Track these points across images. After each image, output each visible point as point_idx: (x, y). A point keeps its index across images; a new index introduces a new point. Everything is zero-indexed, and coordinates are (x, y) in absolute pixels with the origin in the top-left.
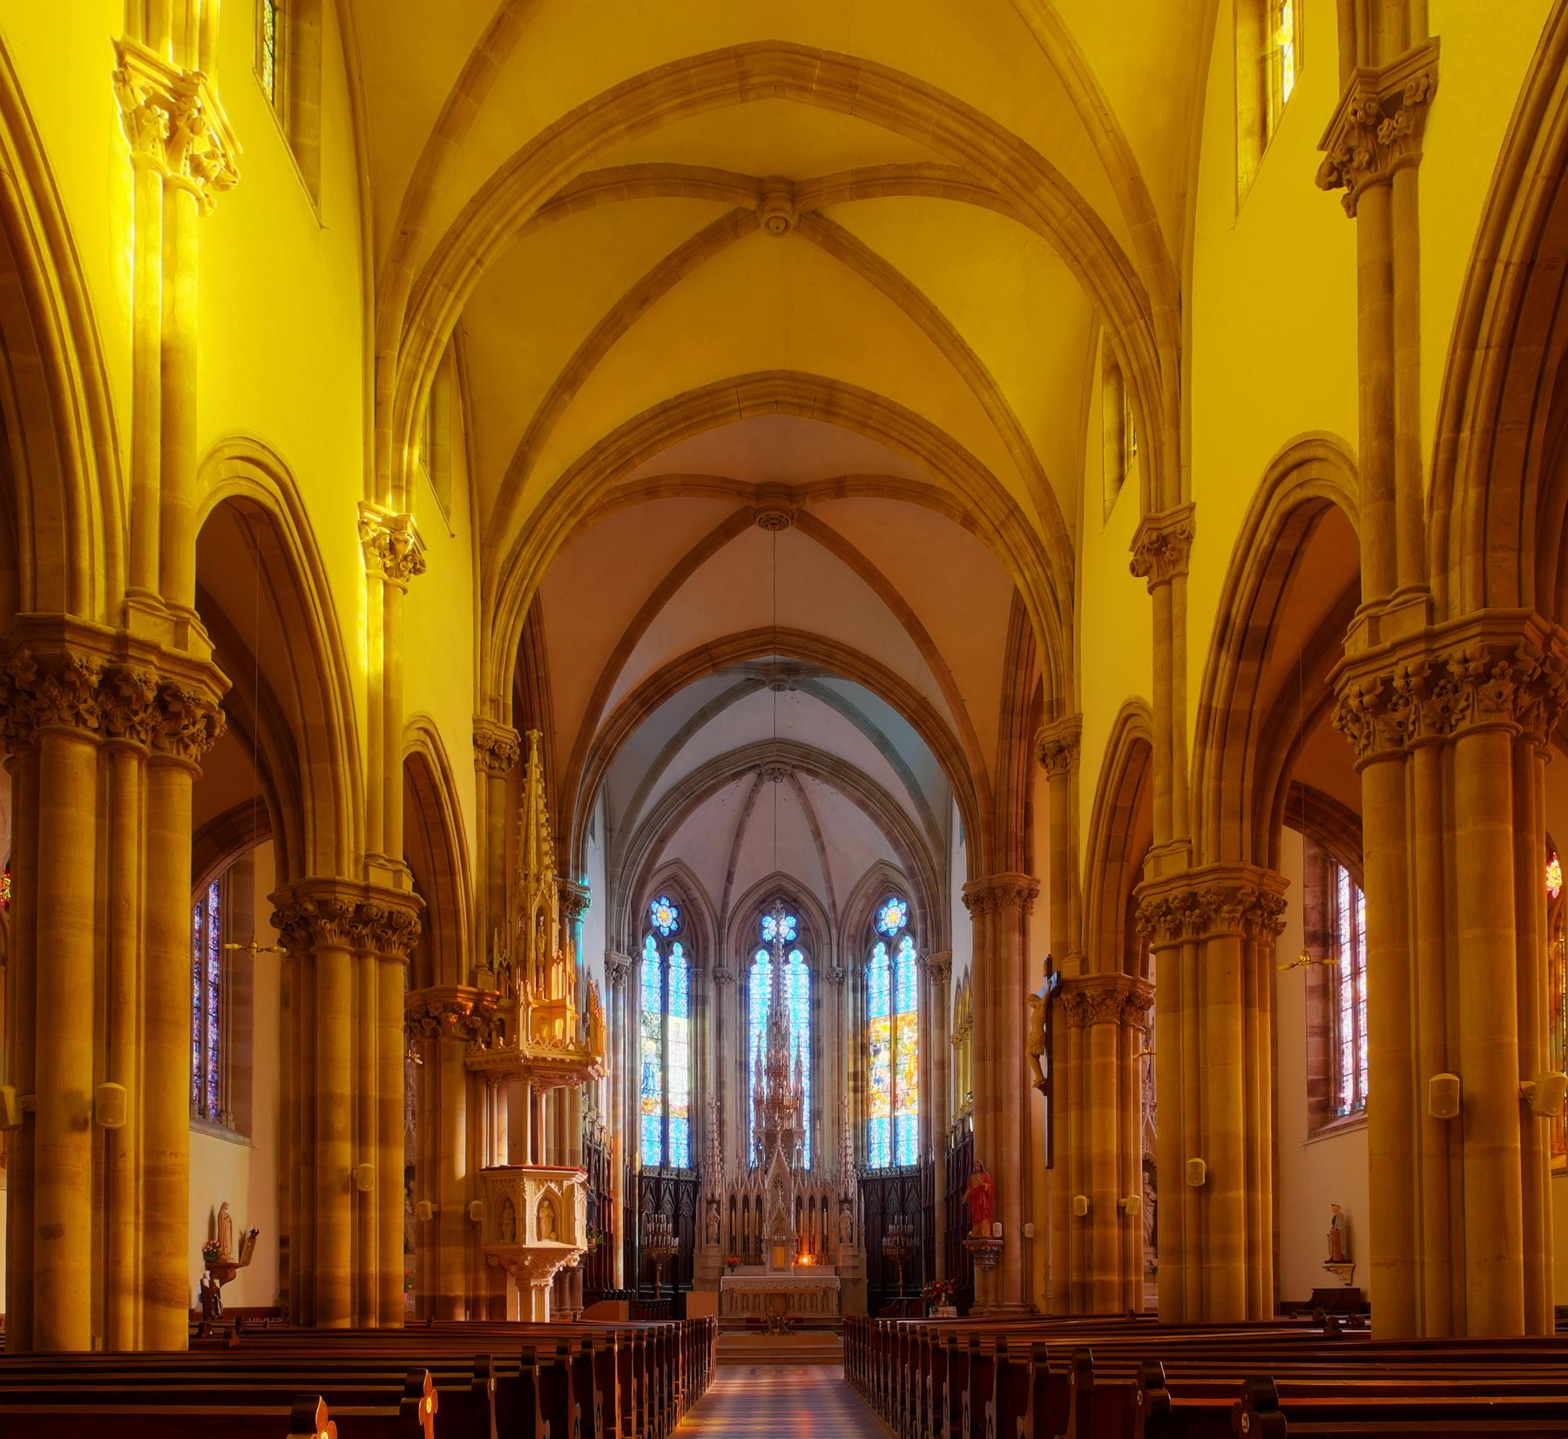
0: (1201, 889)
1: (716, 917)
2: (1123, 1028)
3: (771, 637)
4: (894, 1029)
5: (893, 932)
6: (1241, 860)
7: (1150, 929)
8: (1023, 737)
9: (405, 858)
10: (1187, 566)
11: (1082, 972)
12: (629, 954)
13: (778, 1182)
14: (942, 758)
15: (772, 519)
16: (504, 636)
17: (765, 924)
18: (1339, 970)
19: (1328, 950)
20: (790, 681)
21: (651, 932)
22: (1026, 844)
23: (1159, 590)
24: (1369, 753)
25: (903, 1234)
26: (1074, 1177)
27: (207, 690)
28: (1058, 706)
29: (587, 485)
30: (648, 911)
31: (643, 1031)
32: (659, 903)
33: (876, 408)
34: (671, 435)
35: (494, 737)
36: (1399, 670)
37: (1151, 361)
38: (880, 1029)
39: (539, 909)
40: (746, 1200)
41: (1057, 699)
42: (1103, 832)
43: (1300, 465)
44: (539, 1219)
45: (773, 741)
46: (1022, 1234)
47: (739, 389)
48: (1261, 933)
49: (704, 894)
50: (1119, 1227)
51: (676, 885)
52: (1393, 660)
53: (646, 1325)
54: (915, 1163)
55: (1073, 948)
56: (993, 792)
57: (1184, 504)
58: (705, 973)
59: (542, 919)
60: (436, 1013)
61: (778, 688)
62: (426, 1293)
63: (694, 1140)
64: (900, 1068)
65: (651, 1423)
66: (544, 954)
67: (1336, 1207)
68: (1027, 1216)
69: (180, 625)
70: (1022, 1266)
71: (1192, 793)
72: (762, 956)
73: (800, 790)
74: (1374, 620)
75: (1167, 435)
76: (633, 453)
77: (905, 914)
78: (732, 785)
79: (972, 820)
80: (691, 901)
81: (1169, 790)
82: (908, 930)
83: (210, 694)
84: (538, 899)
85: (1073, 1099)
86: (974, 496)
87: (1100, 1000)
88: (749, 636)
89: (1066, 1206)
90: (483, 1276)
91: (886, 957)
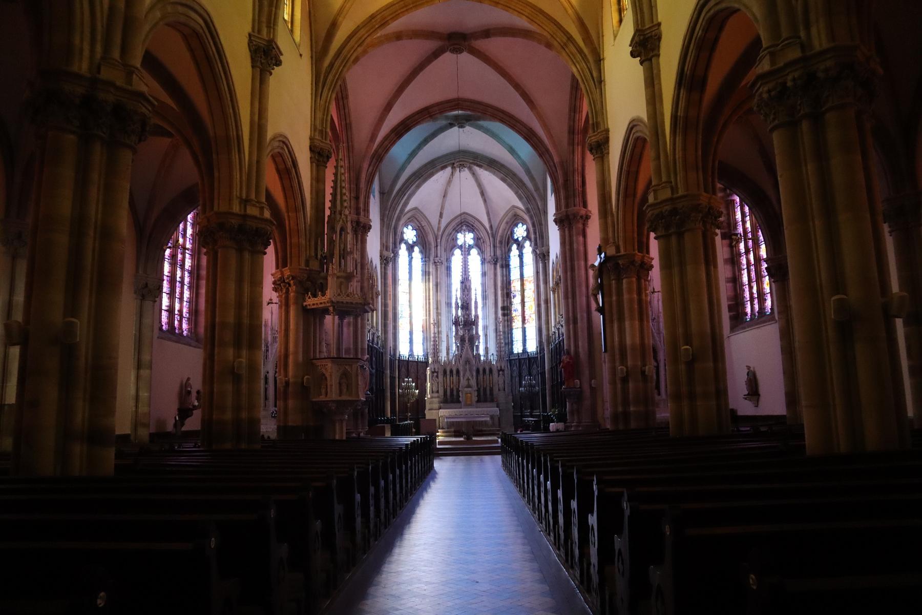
1: (435, 234)
3: (457, 103)
4: (522, 285)
5: (520, 239)
7: (654, 227)
8: (579, 144)
10: (659, 51)
11: (617, 253)
13: (468, 362)
14: (541, 155)
23: (646, 63)
24: (776, 122)
25: (531, 386)
26: (617, 357)
27: (142, 106)
28: (596, 125)
29: (367, 32)
30: (402, 233)
32: (407, 228)
34: (407, 10)
36: (790, 77)
40: (451, 371)
41: (596, 122)
42: (623, 183)
46: (590, 385)
48: (711, 228)
49: (429, 222)
55: (611, 240)
57: (655, 23)
59: (343, 233)
61: (461, 126)
62: (282, 424)
65: (415, 477)
66: (344, 250)
67: (748, 367)
69: (262, 209)
71: (671, 158)
72: (457, 252)
73: (474, 174)
74: (773, 55)
77: (526, 230)
81: (658, 157)
82: (528, 237)
83: (144, 108)
85: (615, 317)
86: (551, 32)
89: (613, 370)
91: (518, 251)
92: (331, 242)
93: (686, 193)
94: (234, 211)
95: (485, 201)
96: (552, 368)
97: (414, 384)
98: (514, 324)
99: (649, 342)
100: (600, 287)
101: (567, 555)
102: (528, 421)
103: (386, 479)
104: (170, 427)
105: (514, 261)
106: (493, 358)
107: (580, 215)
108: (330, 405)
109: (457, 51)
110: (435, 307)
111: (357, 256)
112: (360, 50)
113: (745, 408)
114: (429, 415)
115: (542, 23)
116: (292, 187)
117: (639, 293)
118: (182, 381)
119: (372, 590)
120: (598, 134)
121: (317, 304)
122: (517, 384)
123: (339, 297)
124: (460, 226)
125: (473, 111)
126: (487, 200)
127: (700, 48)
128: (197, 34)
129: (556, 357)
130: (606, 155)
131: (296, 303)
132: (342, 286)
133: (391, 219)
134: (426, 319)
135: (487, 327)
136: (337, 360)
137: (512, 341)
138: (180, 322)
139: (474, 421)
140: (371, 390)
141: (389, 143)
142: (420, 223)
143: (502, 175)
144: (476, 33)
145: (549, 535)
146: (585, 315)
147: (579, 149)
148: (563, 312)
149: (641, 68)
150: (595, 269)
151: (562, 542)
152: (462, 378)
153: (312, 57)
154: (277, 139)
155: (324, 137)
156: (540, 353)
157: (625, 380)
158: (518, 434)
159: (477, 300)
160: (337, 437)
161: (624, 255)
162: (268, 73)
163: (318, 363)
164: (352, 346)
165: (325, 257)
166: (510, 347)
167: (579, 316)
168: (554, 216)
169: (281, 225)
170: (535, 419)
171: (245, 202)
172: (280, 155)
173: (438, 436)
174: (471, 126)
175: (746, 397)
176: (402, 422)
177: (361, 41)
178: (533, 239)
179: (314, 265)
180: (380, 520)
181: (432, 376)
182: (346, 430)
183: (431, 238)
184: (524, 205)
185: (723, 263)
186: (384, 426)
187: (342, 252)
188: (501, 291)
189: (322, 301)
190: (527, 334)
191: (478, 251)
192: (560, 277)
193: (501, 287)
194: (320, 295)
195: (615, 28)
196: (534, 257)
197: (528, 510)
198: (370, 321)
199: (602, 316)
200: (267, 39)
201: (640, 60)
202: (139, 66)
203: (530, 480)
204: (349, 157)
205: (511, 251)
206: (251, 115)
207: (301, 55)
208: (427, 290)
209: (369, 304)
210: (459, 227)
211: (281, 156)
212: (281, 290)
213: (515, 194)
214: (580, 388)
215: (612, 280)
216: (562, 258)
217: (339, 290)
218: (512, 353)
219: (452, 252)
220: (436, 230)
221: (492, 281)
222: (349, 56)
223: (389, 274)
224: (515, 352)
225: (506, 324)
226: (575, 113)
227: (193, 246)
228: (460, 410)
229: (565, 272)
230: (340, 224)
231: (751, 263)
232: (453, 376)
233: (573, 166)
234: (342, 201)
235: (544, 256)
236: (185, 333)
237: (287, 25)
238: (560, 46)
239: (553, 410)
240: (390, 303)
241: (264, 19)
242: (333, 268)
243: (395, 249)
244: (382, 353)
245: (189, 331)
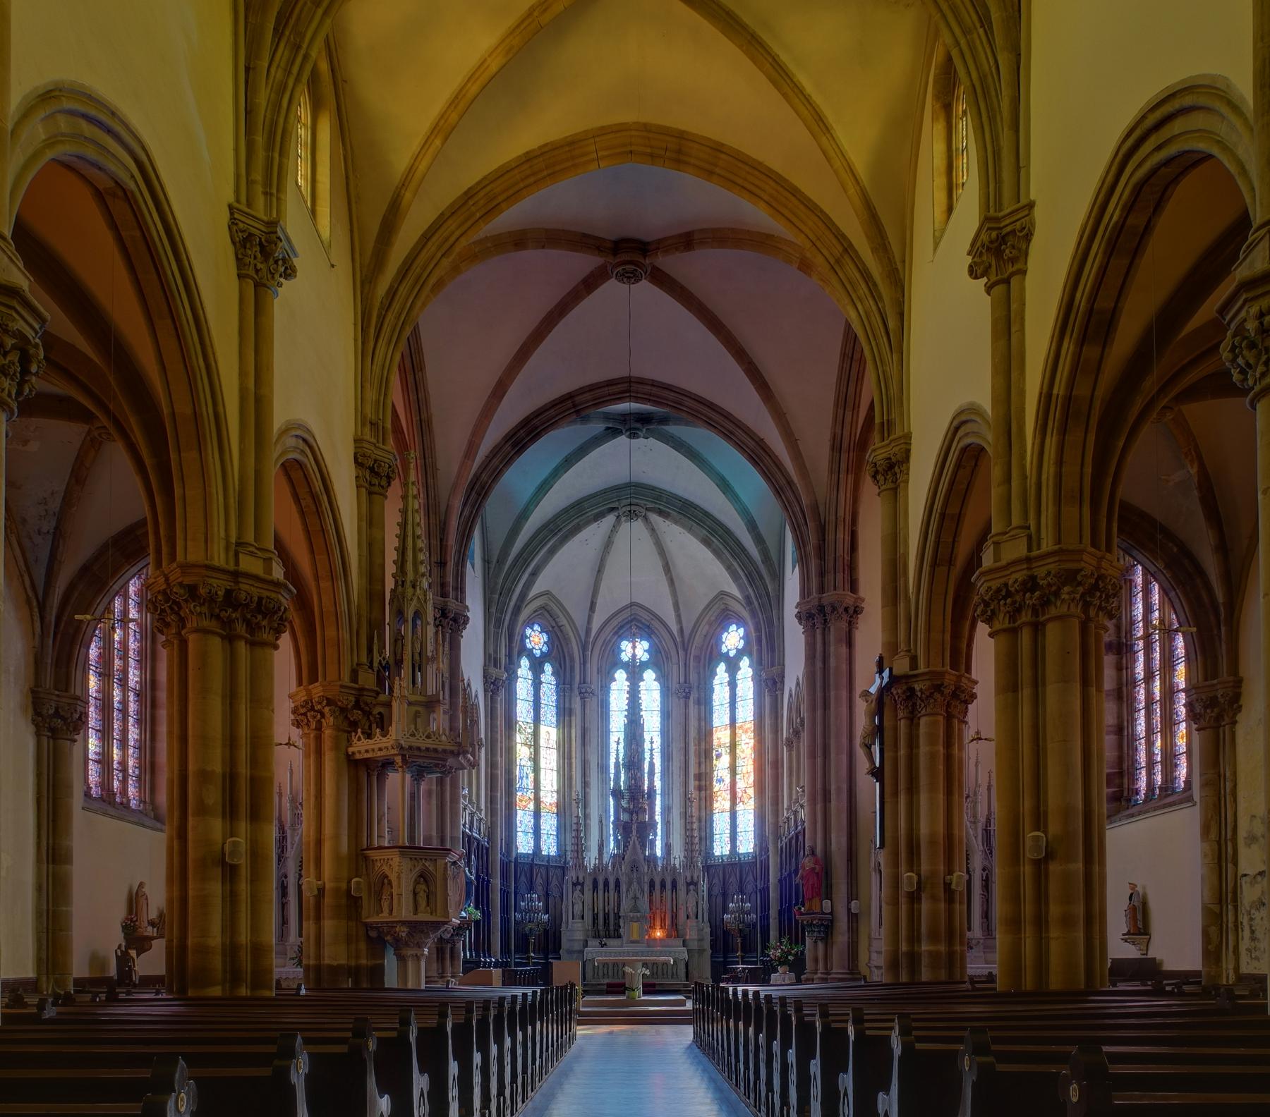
0: (1040, 572)
3: (627, 387)
5: (732, 654)
6: (1081, 542)
7: (989, 613)
9: (275, 548)
10: (1026, 263)
13: (634, 867)
14: (778, 492)
15: (627, 273)
16: (383, 366)
17: (623, 647)
18: (1133, 674)
19: (1122, 658)
20: (644, 430)
21: (526, 653)
22: (852, 567)
23: (999, 289)
25: (741, 911)
28: (887, 426)
30: (522, 635)
31: (519, 738)
32: (532, 628)
33: (723, 156)
35: (374, 456)
37: (990, 68)
38: (721, 736)
39: (415, 613)
42: (932, 537)
44: (415, 894)
45: (629, 485)
46: (849, 910)
47: (597, 139)
48: (1097, 615)
50: (945, 901)
52: (1008, 572)
53: (518, 991)
54: (752, 851)
55: (903, 646)
56: (823, 522)
57: (1023, 201)
58: (571, 689)
59: (419, 622)
60: (319, 707)
61: (633, 436)
64: (739, 770)
66: (420, 654)
67: (1133, 886)
68: (852, 895)
69: (268, 561)
70: (849, 938)
71: (1031, 481)
73: (653, 531)
76: (501, 198)
80: (559, 627)
83: (22, 322)
84: (415, 602)
86: (811, 236)
87: (928, 694)
88: (607, 386)
90: (363, 946)
91: (727, 675)
92: (398, 639)
93: (1057, 547)
94: (216, 563)
95: (671, 582)
98: (716, 805)
105: (720, 694)
107: (845, 605)
108: (397, 929)
109: (629, 277)
111: (444, 665)
116: (323, 530)
117: (948, 744)
121: (373, 750)
123: (412, 739)
125: (656, 403)
127: (1112, 248)
128: (124, 190)
130: (902, 485)
131: (336, 747)
132: (419, 720)
133: (502, 611)
136: (410, 850)
138: (124, 782)
141: (501, 463)
143: (705, 532)
144: (665, 239)
150: (870, 700)
154: (294, 433)
157: (914, 898)
161: (923, 674)
164: (434, 833)
165: (386, 667)
167: (833, 788)
168: (796, 608)
169: (303, 602)
179: (368, 680)
182: (426, 977)
187: (417, 657)
192: (802, 721)
194: (378, 735)
199: (878, 784)
200: (265, 218)
209: (467, 752)
212: (308, 724)
213: (727, 570)
214: (831, 913)
217: (413, 726)
222: (425, 275)
224: (716, 854)
227: (142, 645)
229: (813, 709)
232: (608, 891)
235: (775, 683)
236: (133, 804)
241: (258, 176)
242: (402, 685)
243: (512, 666)
244: (487, 849)
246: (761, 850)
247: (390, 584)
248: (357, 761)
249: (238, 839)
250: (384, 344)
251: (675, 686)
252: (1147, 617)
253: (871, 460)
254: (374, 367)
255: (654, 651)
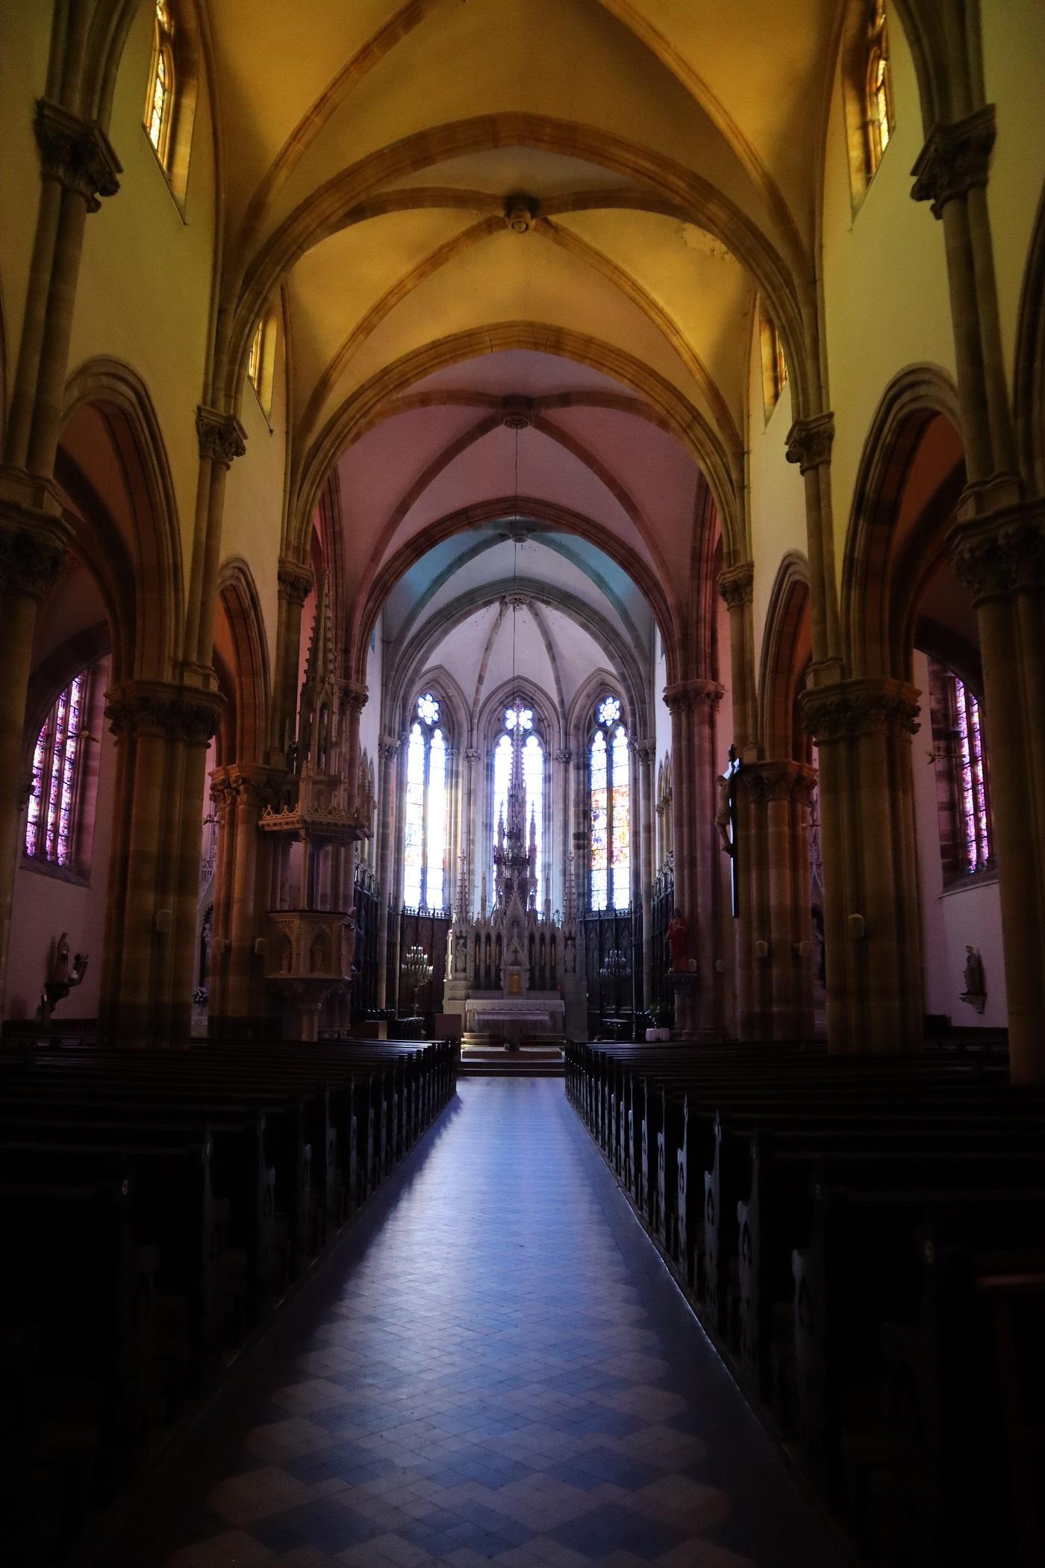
2: (793, 803)
4: (610, 799)
5: (609, 723)
8: (708, 578)
11: (759, 760)
12: (399, 739)
13: (515, 922)
14: (646, 593)
15: (515, 421)
21: (418, 721)
23: (809, 473)
25: (618, 965)
26: (755, 925)
28: (734, 555)
34: (440, 363)
36: (1002, 532)
40: (488, 937)
41: (734, 550)
42: (772, 650)
43: (912, 386)
47: (490, 332)
51: (438, 686)
57: (825, 412)
58: (459, 753)
61: (519, 539)
63: (447, 885)
65: (429, 1104)
66: (326, 739)
67: (969, 949)
69: (206, 678)
72: (505, 741)
73: (536, 615)
74: (979, 497)
75: (809, 365)
77: (619, 709)
78: (483, 611)
79: (670, 640)
82: (621, 721)
86: (666, 405)
91: (604, 743)
94: (165, 680)
95: (553, 659)
96: (653, 939)
97: (426, 956)
98: (594, 863)
99: (809, 901)
100: (732, 813)
101: (651, 1215)
102: (612, 1023)
103: (389, 1099)
104: (32, 1013)
105: (598, 760)
106: (558, 918)
107: (706, 691)
108: (295, 986)
110: (465, 828)
111: (345, 749)
112: (363, 421)
113: (964, 1015)
114: (449, 1008)
115: (652, 389)
118: (53, 938)
119: (350, 1286)
120: (735, 570)
121: (280, 824)
122: (596, 963)
124: (512, 697)
126: (556, 656)
128: (124, 414)
129: (661, 921)
134: (450, 849)
135: (549, 865)
136: (310, 913)
137: (590, 891)
138: (55, 842)
139: (522, 1021)
140: (357, 963)
141: (402, 565)
142: (445, 690)
145: (630, 1190)
146: (709, 854)
147: (707, 589)
148: (673, 847)
149: (802, 479)
151: (645, 1196)
152: (505, 949)
153: (287, 433)
155: (301, 559)
156: (636, 912)
157: (766, 963)
158: (595, 1043)
159: (535, 822)
160: (304, 1038)
162: (225, 467)
163: (279, 918)
165: (296, 750)
166: (586, 900)
167: (699, 854)
168: (664, 691)
170: (623, 1021)
171: (182, 666)
172: (234, 588)
173: (465, 1043)
174: (534, 538)
175: (964, 996)
176: (405, 1018)
177: (366, 408)
178: (630, 726)
179: (278, 761)
180: (380, 1158)
181: (457, 944)
182: (319, 1027)
183: (462, 716)
184: (617, 668)
185: (934, 779)
186: (378, 1023)
187: (323, 743)
188: (575, 807)
189: (289, 820)
190: (615, 879)
191: (539, 741)
192: (671, 789)
193: (575, 800)
194: (285, 811)
195: (766, 407)
196: (631, 753)
197: (601, 1159)
198: (359, 851)
199: (732, 859)
200: (225, 415)
201: (800, 467)
202: (51, 477)
203: (606, 1112)
204: (336, 587)
205: (594, 741)
206: (195, 530)
207: (271, 431)
208: (453, 802)
209: (364, 827)
210: (510, 699)
211: (235, 590)
215: (750, 803)
216: (674, 760)
217: (316, 804)
218: (590, 910)
219: (496, 741)
220: (471, 705)
221: (561, 791)
223: (392, 774)
224: (594, 909)
225: (581, 863)
226: (702, 528)
228: (501, 1001)
229: (679, 781)
230: (321, 699)
231: (978, 781)
232: (490, 946)
233: (698, 612)
234: (326, 661)
235: (647, 754)
236: (61, 860)
237: (252, 383)
238: (681, 429)
239: (651, 1007)
240: (392, 821)
241: (221, 384)
242: (309, 768)
244: (376, 904)
245: (67, 858)
246: (636, 908)
247: (302, 678)
248: (265, 832)
249: (166, 911)
250: (309, 484)
251: (555, 752)
252: (969, 709)
253: (720, 581)
254: (299, 503)
255: (538, 720)
